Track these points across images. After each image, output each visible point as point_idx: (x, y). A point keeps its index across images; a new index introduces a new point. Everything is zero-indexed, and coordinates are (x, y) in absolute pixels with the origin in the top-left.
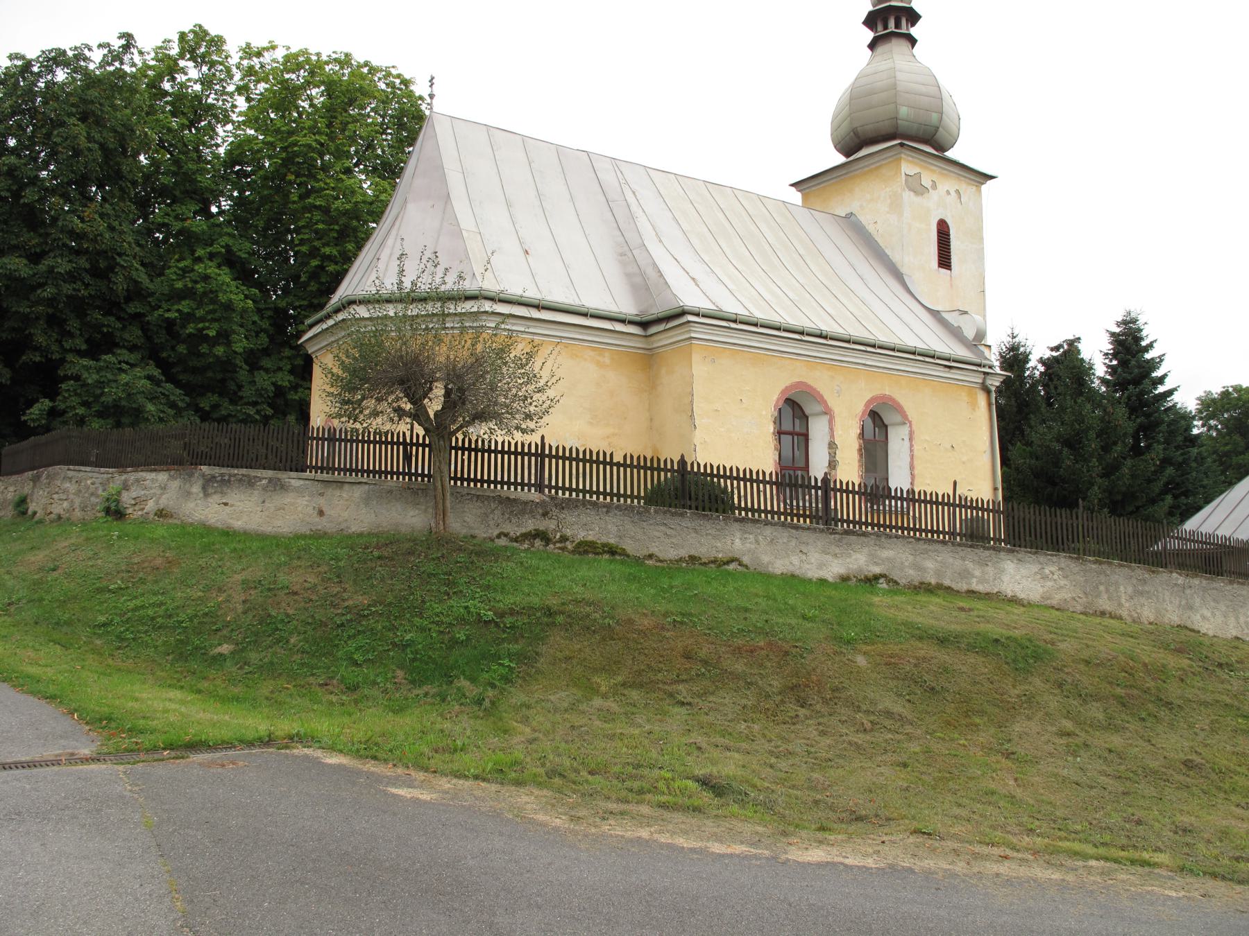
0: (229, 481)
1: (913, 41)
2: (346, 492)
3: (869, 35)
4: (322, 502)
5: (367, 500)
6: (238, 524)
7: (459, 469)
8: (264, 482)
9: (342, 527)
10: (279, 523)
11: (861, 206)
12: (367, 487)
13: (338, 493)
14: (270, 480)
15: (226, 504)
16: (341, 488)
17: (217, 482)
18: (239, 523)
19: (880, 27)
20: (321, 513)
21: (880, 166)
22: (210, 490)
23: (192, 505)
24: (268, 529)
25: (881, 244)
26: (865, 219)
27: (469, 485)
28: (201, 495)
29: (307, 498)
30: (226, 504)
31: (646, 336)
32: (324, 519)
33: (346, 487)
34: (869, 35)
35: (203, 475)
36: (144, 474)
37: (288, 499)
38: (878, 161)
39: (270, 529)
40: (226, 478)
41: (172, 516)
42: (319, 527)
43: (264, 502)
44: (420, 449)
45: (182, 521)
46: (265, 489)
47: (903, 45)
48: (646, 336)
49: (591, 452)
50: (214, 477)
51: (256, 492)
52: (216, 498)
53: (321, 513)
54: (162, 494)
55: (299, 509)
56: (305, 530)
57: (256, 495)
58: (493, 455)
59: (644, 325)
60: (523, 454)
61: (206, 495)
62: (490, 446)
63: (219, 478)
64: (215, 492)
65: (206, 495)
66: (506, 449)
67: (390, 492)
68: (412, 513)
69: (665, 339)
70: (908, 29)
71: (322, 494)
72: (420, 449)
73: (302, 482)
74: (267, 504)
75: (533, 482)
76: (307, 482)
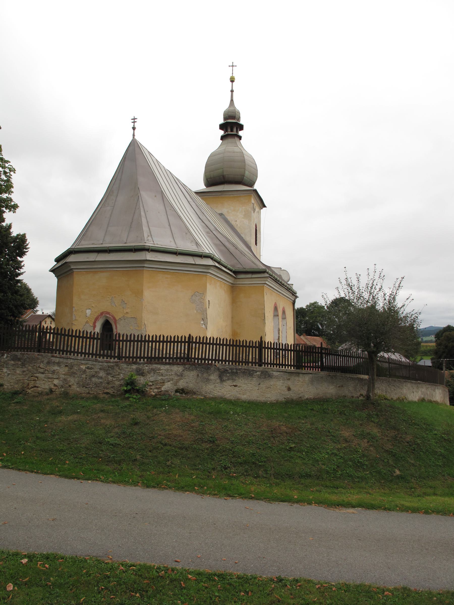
0: (237, 373)
1: (240, 138)
2: (301, 378)
3: (222, 133)
4: (289, 383)
5: (312, 382)
6: (244, 397)
7: (80, 347)
8: (258, 373)
9: (300, 396)
10: (269, 395)
11: (228, 212)
12: (311, 375)
13: (297, 378)
14: (262, 372)
15: (235, 386)
16: (298, 376)
17: (229, 373)
18: (245, 396)
19: (229, 130)
20: (289, 389)
21: (240, 196)
22: (225, 378)
23: (212, 387)
24: (262, 399)
25: (239, 232)
26: (230, 218)
27: (229, 364)
28: (218, 381)
29: (281, 381)
30: (235, 386)
31: (235, 278)
32: (291, 392)
33: (301, 375)
34: (222, 133)
35: (218, 369)
36: (159, 366)
37: (272, 382)
38: (239, 194)
39: (264, 399)
40: (235, 371)
41: (195, 393)
42: (288, 397)
43: (259, 384)
44: (201, 345)
45: (205, 396)
46: (259, 377)
47: (237, 139)
48: (235, 278)
49: (164, 336)
50: (227, 370)
51: (254, 379)
52: (229, 382)
53: (289, 389)
54: (180, 379)
55: (278, 387)
56: (281, 399)
57: (255, 381)
58: (74, 338)
59: (235, 272)
60: (240, 346)
61: (222, 381)
62: (268, 346)
63: (230, 371)
64: (228, 379)
65: (222, 381)
66: (225, 343)
67: (322, 378)
68: (331, 387)
69: (245, 281)
70: (237, 132)
71: (289, 379)
72: (201, 345)
73: (279, 373)
74: (261, 386)
75: (292, 364)
76: (281, 373)
